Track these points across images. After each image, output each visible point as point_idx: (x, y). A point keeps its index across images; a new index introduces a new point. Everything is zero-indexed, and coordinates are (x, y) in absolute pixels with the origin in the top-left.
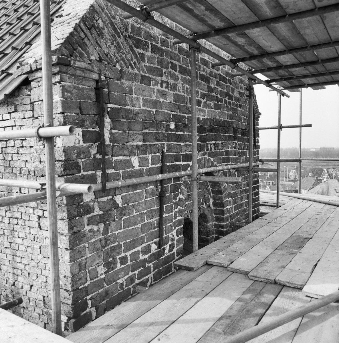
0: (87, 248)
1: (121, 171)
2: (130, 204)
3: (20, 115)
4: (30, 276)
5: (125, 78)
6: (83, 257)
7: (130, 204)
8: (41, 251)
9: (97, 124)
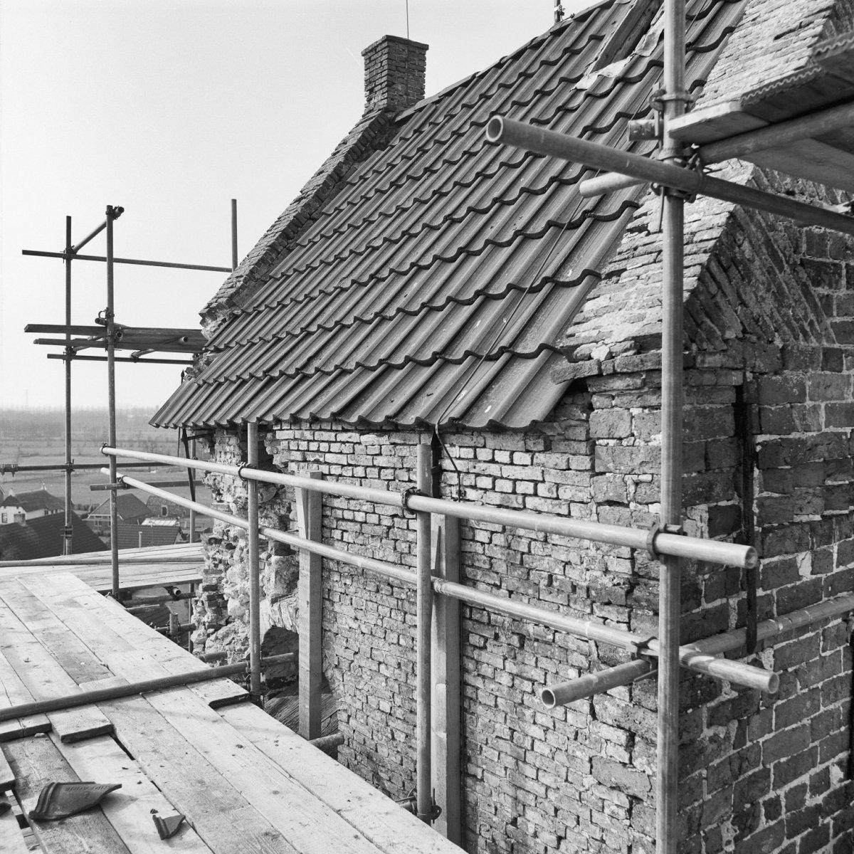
0: (704, 781)
1: (775, 591)
2: (790, 670)
3: (559, 461)
4: (560, 817)
5: (791, 365)
6: (695, 801)
7: (790, 670)
8: (592, 767)
9: (736, 489)
